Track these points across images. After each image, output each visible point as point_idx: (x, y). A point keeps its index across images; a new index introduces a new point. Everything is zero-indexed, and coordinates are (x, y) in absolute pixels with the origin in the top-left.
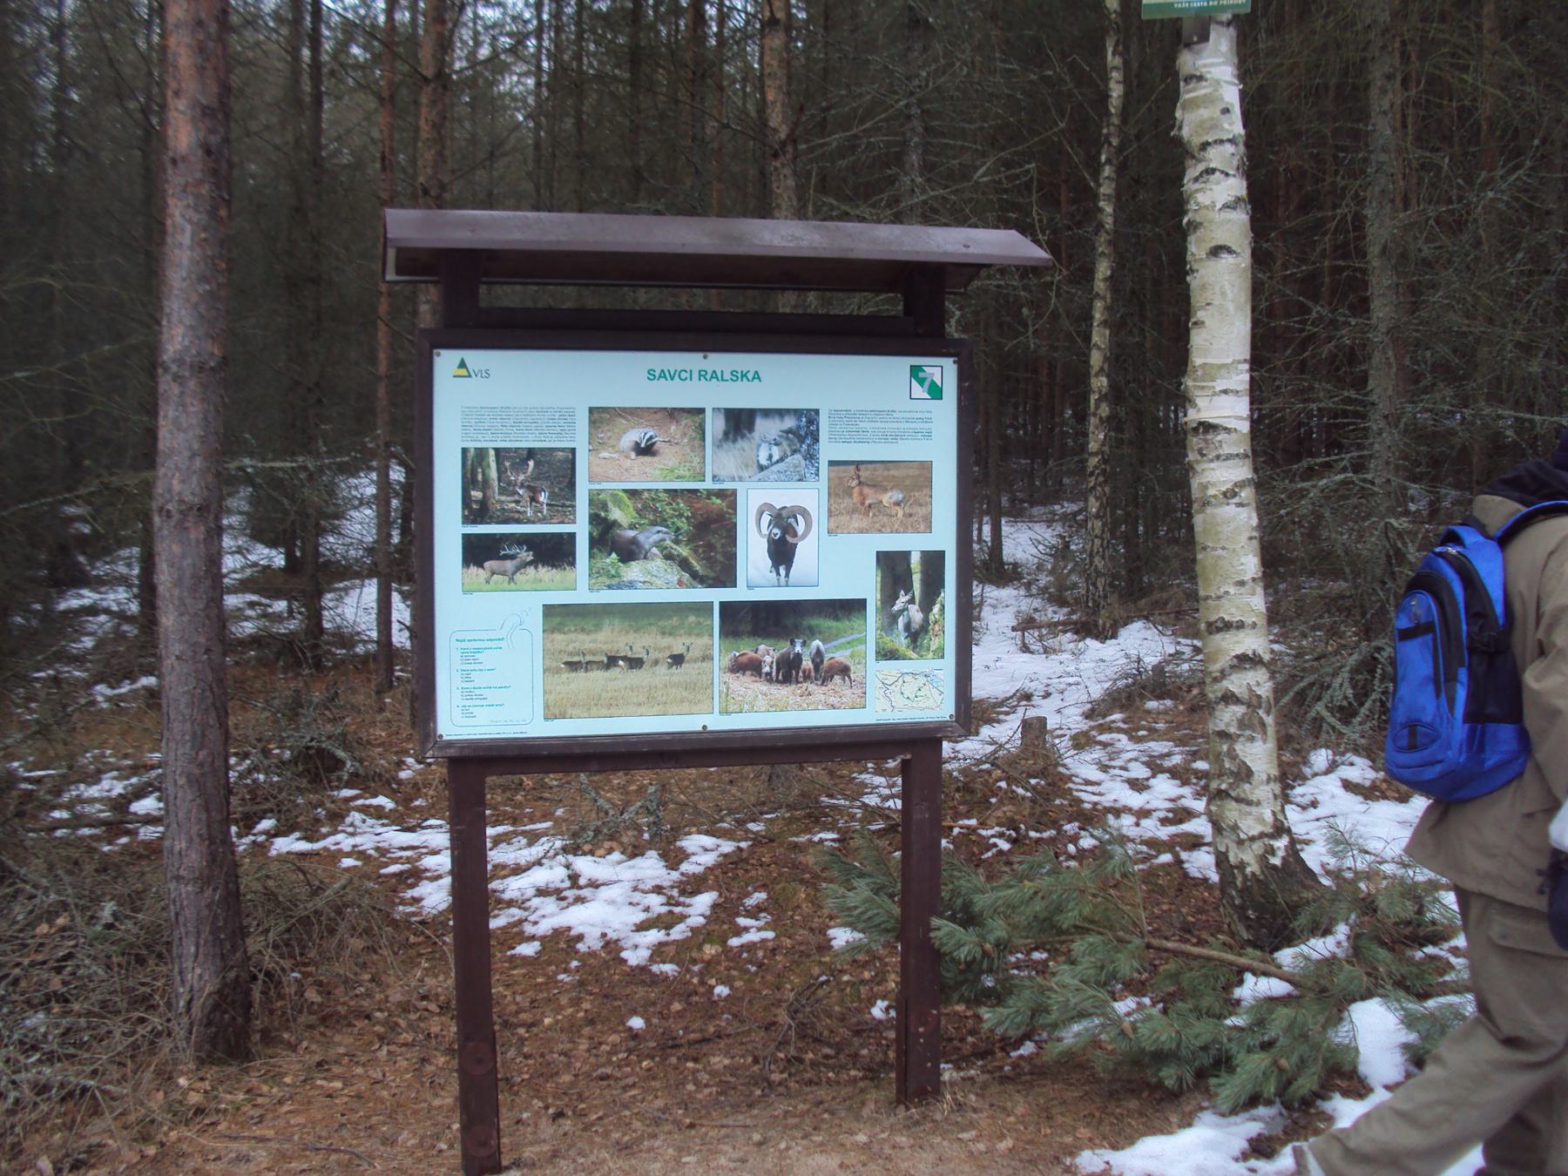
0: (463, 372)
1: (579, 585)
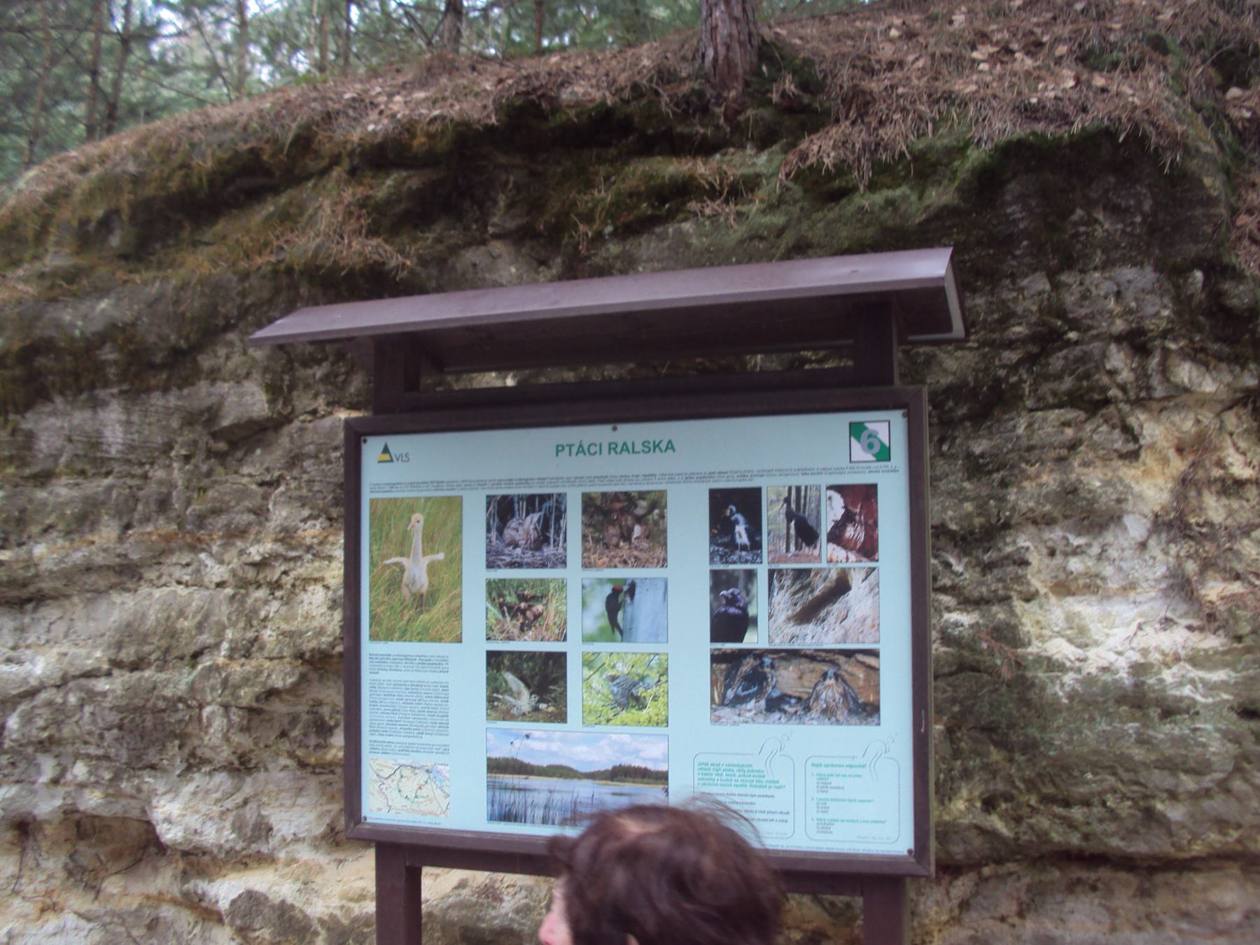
0: (387, 457)
1: (323, 778)
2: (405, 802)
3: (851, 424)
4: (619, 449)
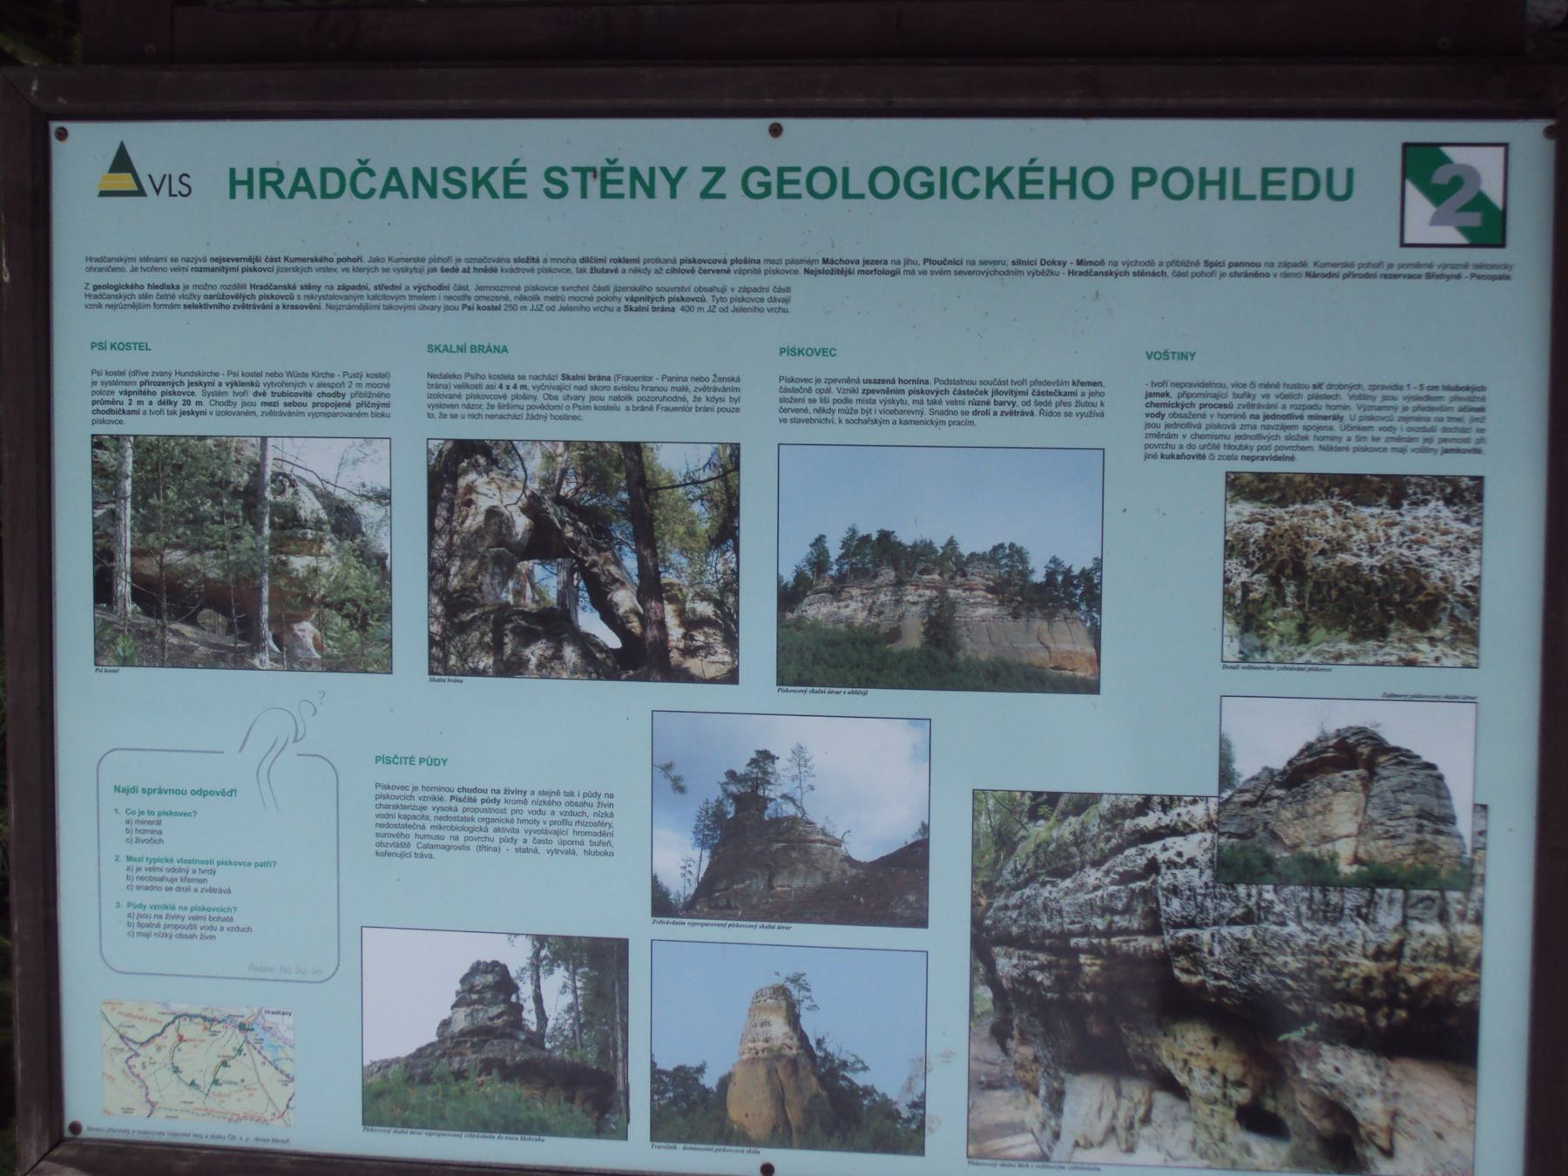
0: (124, 181)
2: (189, 1094)
3: (1406, 146)
4: (286, 187)
